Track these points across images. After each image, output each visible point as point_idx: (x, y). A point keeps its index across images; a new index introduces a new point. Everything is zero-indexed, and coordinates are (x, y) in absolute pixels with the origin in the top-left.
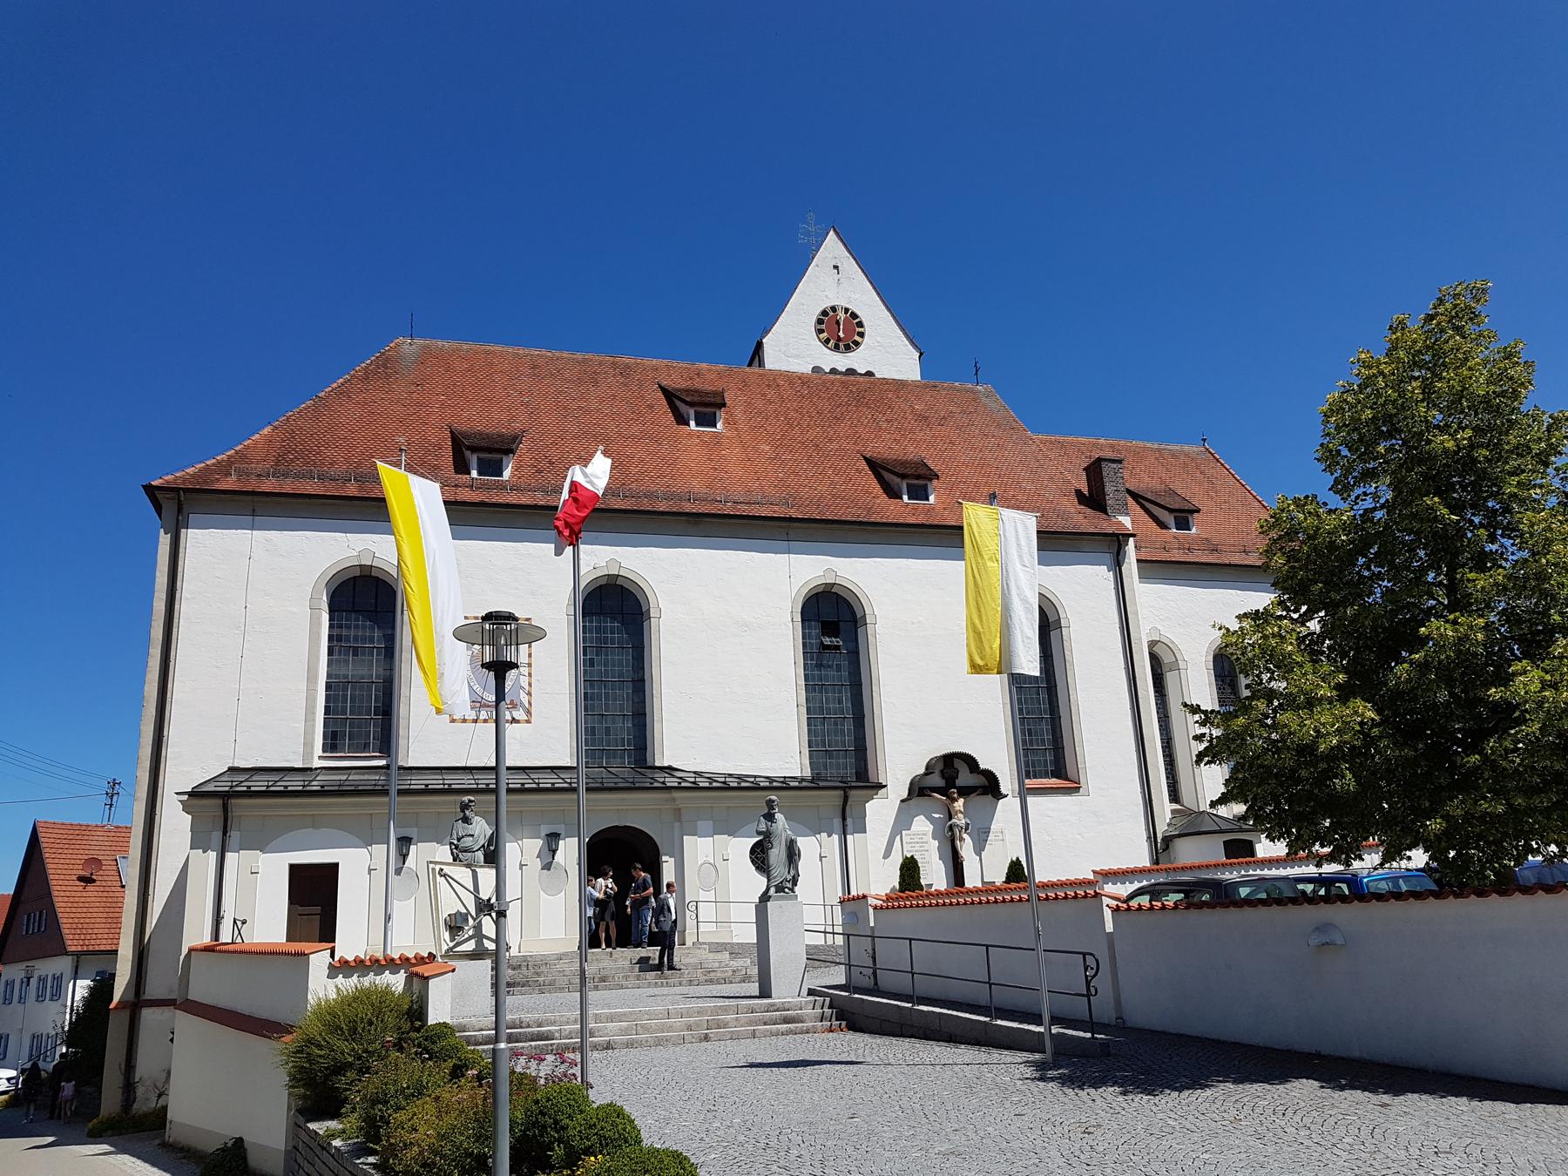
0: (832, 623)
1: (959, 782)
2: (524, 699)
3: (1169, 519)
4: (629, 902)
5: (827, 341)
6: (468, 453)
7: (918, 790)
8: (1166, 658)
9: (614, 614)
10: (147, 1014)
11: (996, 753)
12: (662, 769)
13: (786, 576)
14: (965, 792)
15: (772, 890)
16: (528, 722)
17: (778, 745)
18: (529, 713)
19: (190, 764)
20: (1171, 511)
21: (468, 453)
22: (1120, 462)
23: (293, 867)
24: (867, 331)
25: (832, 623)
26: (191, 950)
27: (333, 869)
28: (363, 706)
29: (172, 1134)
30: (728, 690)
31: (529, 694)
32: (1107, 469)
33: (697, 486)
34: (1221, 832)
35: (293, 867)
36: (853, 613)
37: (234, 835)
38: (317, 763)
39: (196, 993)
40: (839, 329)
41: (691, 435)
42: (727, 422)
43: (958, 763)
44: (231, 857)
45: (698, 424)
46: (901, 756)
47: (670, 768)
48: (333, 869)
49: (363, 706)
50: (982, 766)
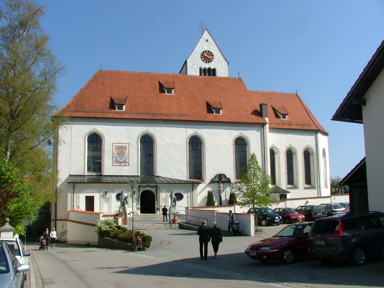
0: (196, 144)
1: (222, 180)
2: (128, 161)
3: (281, 116)
4: (148, 204)
5: (204, 60)
6: (115, 105)
7: (212, 182)
8: (276, 151)
9: (147, 143)
10: (58, 222)
11: (231, 173)
12: (156, 176)
13: (186, 132)
14: (223, 182)
15: (172, 207)
16: (128, 166)
17: (182, 172)
18: (129, 164)
19: (63, 176)
20: (281, 114)
21: (115, 105)
22: (266, 104)
23: (86, 196)
24: (215, 57)
25: (196, 144)
26: (69, 211)
27: (93, 197)
28: (95, 163)
29: (68, 243)
30: (171, 162)
31: (129, 160)
32: (263, 106)
33: (166, 111)
34: (279, 192)
35: (86, 196)
36: (201, 142)
37: (75, 190)
38: (86, 174)
39: (71, 218)
40: (207, 57)
41: (166, 96)
42: (175, 92)
43: (222, 176)
44: (75, 195)
45: (168, 93)
46: (209, 173)
47: (159, 176)
48: (93, 197)
49: (95, 163)
50: (227, 177)
